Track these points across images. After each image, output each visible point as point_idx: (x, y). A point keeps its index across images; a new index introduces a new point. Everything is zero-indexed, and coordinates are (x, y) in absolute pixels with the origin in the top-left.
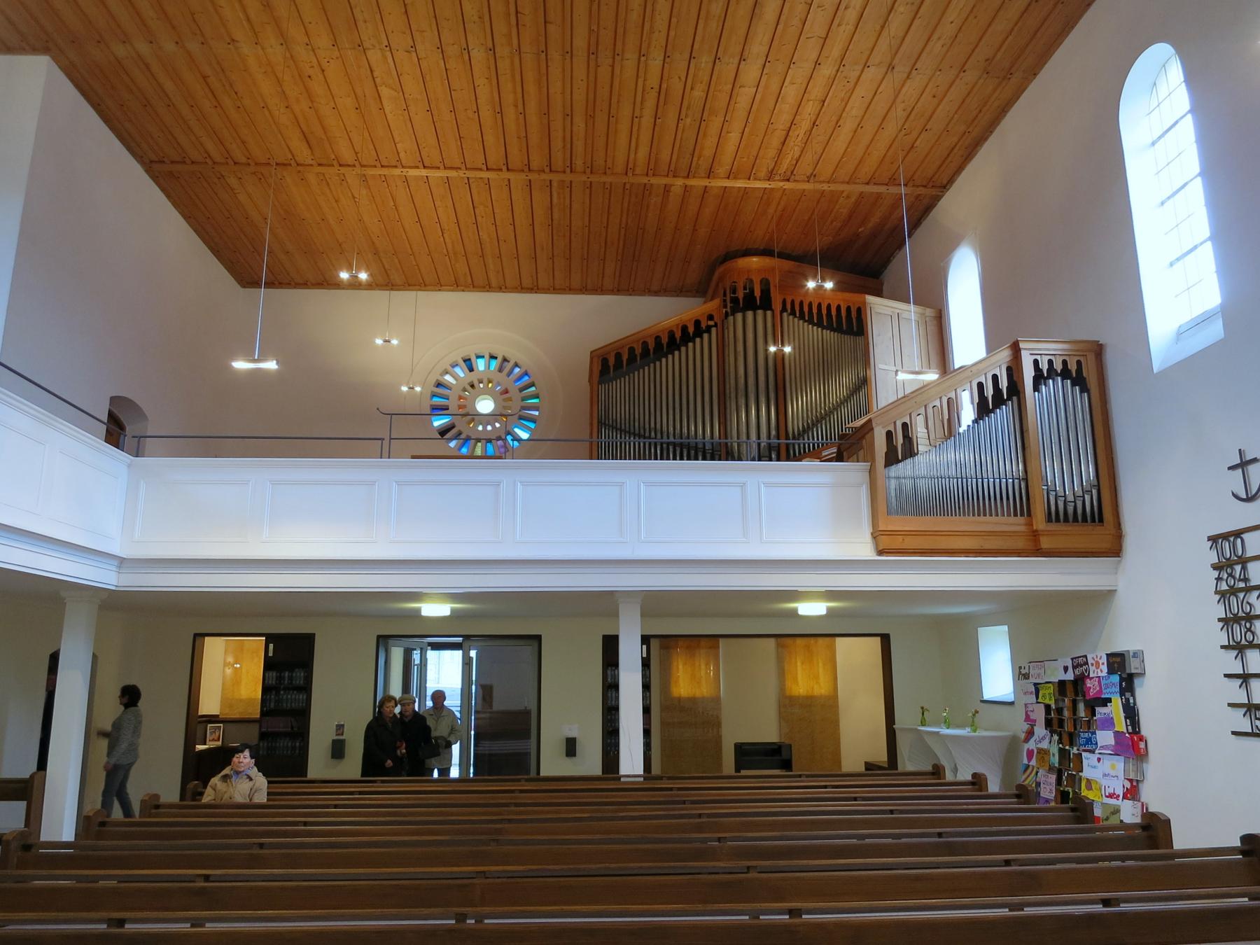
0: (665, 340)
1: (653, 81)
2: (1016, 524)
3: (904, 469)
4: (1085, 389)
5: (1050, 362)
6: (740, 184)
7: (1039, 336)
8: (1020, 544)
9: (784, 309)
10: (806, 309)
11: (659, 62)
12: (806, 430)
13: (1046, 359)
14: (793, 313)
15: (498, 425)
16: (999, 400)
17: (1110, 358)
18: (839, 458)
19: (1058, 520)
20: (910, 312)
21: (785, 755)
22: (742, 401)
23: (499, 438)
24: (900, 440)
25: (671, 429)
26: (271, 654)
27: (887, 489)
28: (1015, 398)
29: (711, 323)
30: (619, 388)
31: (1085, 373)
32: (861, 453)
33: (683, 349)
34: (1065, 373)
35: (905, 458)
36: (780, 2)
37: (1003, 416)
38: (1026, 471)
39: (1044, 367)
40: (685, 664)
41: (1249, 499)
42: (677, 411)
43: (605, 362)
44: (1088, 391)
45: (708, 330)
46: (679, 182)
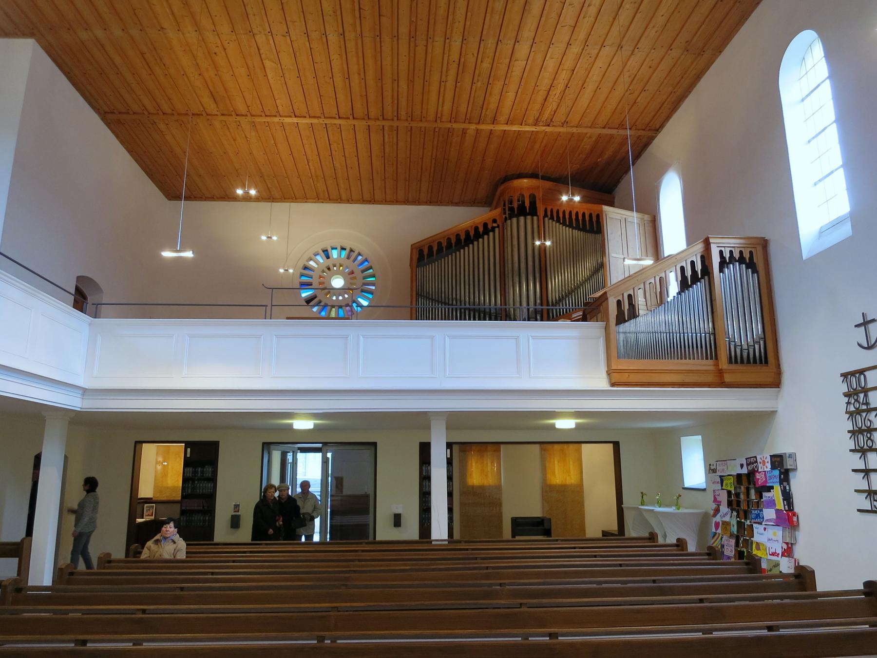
0: (463, 237)
1: (455, 56)
2: (707, 365)
3: (629, 326)
4: (755, 271)
5: (731, 252)
6: (515, 128)
7: (723, 234)
8: (710, 379)
9: (546, 215)
10: (561, 215)
11: (458, 43)
12: (561, 300)
13: (728, 250)
14: (552, 218)
15: (346, 296)
16: (695, 279)
17: (773, 249)
18: (584, 319)
19: (736, 362)
20: (634, 217)
21: (546, 526)
22: (517, 280)
23: (347, 305)
24: (627, 307)
25: (467, 299)
26: (188, 455)
27: (618, 341)
28: (706, 277)
29: (495, 225)
30: (431, 270)
31: (755, 260)
32: (599, 316)
33: (476, 243)
34: (741, 260)
35: (630, 319)
36: (543, 2)
37: (698, 290)
38: (714, 328)
39: (727, 255)
40: (477, 462)
41: (870, 348)
42: (472, 286)
43: (421, 252)
44: (757, 272)
45: (493, 229)
46: (473, 127)
